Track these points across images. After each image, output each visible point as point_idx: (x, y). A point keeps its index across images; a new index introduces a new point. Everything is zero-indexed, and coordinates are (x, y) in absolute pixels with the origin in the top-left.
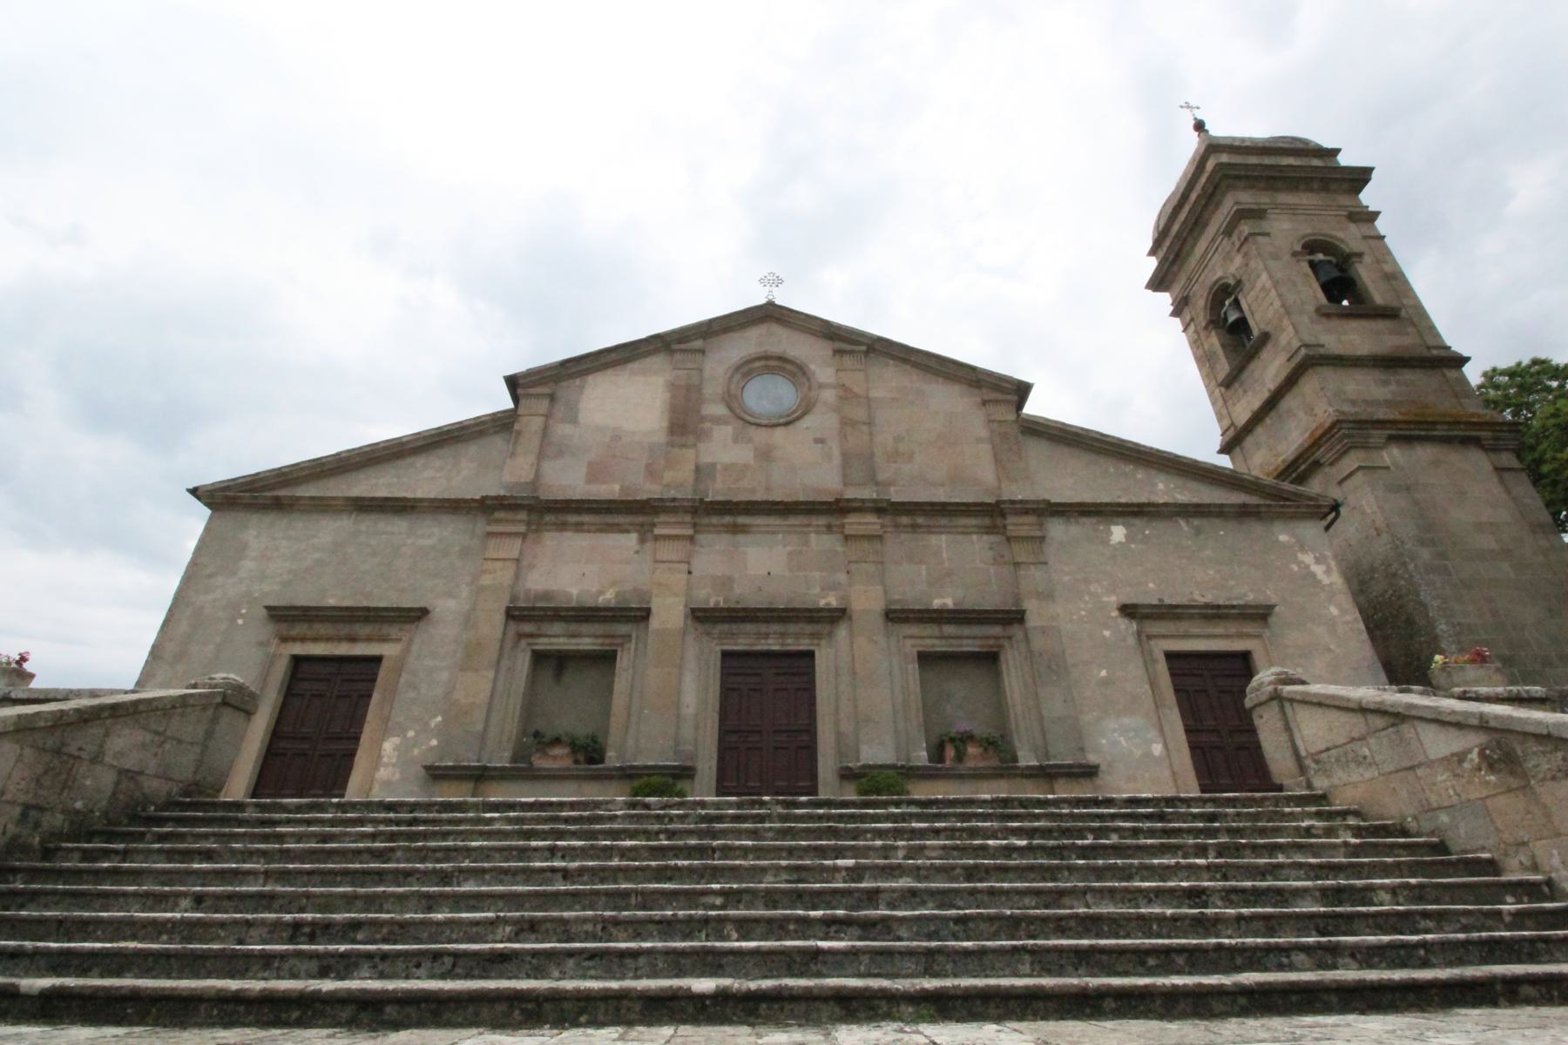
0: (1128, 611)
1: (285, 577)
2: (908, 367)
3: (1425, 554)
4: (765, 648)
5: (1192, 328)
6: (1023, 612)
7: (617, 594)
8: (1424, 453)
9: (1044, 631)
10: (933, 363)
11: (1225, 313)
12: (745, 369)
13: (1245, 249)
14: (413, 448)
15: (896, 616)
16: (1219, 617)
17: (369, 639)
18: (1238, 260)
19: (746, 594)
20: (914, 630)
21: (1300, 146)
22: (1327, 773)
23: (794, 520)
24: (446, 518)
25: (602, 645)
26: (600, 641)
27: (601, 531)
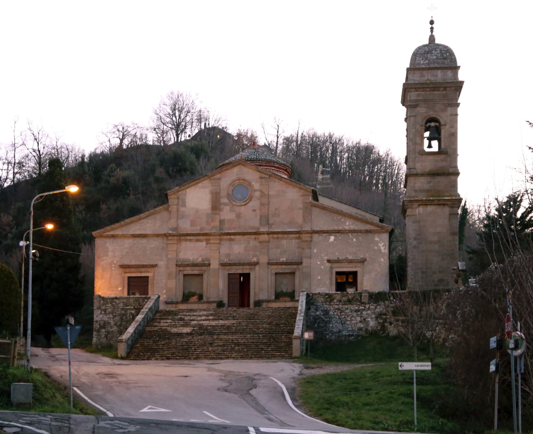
0: (329, 261)
17: (145, 272)
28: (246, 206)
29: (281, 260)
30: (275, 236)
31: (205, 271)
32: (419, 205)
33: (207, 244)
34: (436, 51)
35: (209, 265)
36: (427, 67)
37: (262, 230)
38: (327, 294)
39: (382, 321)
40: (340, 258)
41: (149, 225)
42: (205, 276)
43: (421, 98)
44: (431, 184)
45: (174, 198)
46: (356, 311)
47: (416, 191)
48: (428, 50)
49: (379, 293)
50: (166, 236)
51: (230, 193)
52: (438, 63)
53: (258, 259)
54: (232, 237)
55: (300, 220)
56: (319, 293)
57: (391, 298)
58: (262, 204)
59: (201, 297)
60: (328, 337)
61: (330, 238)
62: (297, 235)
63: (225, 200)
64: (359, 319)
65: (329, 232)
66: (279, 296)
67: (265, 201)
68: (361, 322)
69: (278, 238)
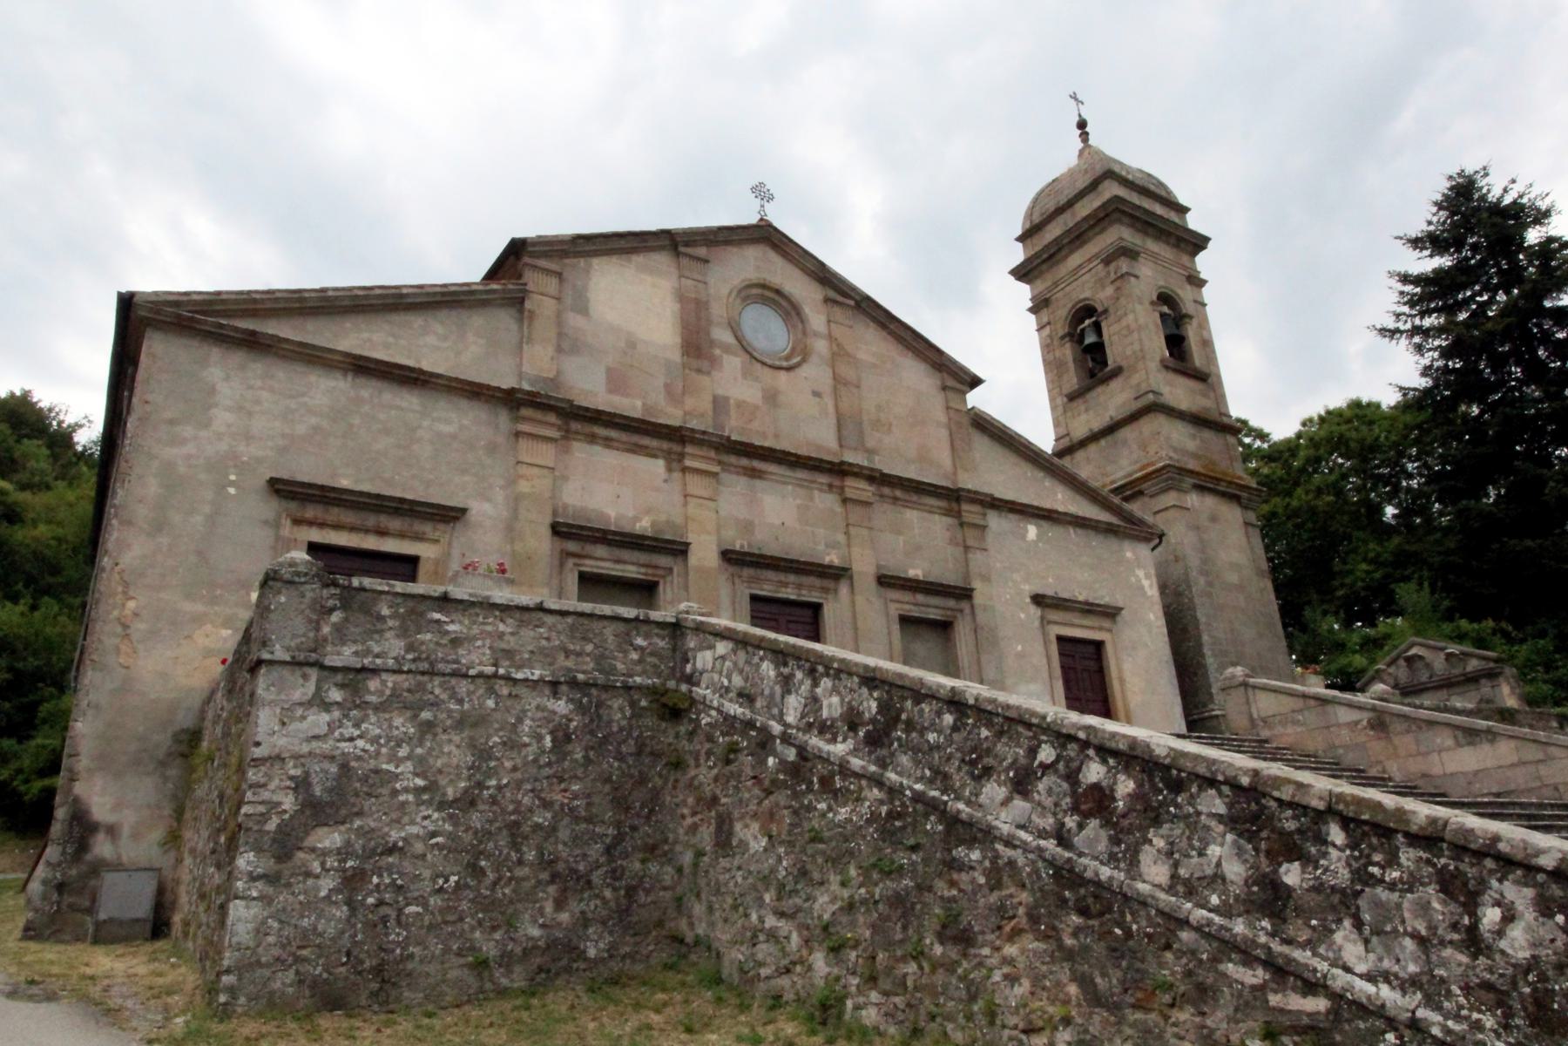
0: (1038, 600)
1: (281, 442)
2: (884, 333)
3: (1202, 581)
4: (785, 596)
5: (1047, 331)
6: (972, 590)
7: (653, 524)
8: (1210, 501)
9: (985, 608)
10: (908, 337)
11: (1083, 330)
12: (743, 294)
13: (1118, 283)
14: (411, 304)
15: (886, 581)
16: (1089, 612)
17: (402, 535)
18: (1110, 290)
19: (766, 541)
20: (907, 596)
21: (1163, 194)
22: (1270, 728)
23: (801, 474)
24: (464, 403)
25: (646, 574)
26: (643, 570)
27: (628, 451)
28: (792, 374)
33: (669, 470)
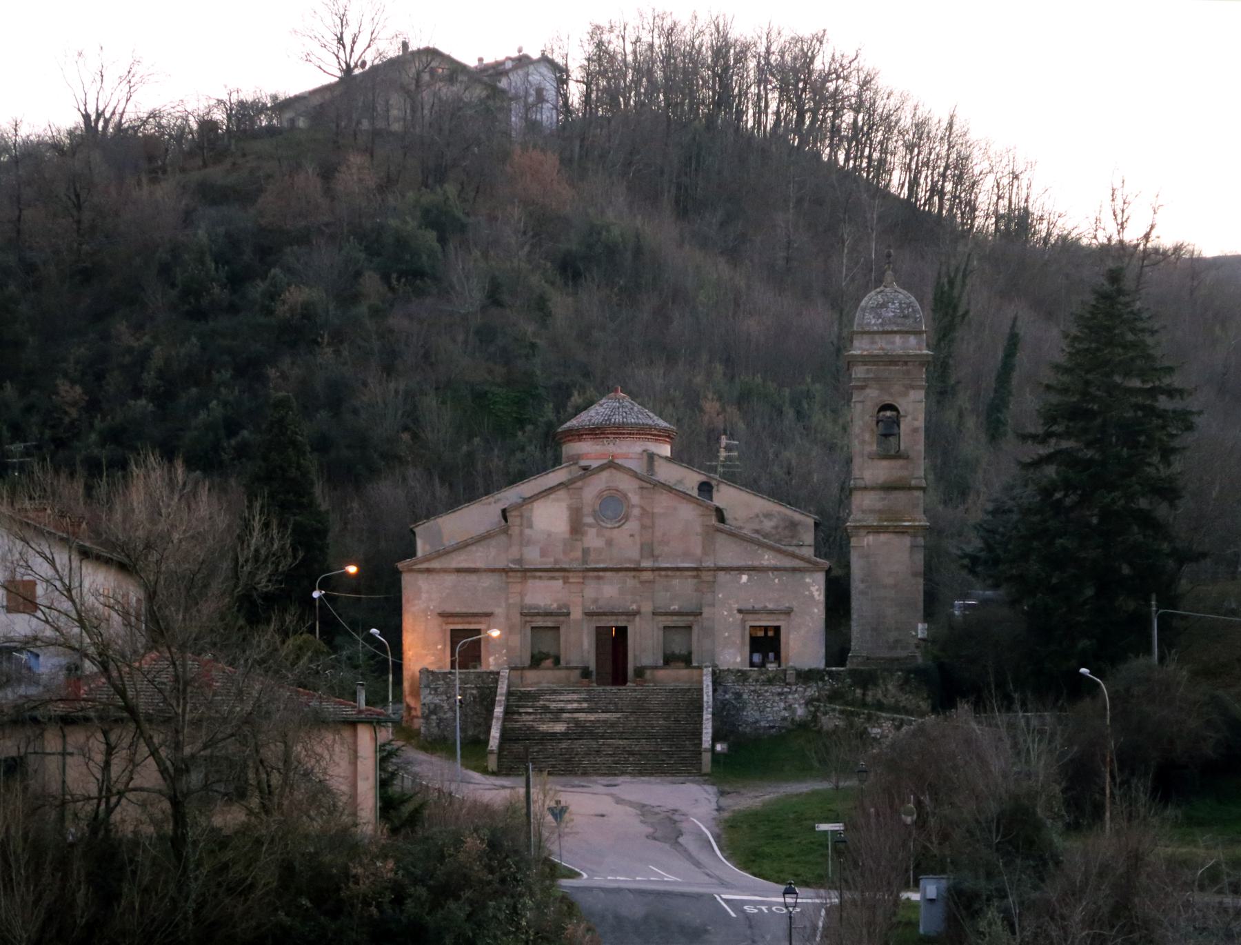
0: (740, 611)
17: (475, 623)
29: (672, 608)
30: (663, 573)
31: (563, 622)
32: (869, 532)
33: (565, 583)
34: (893, 303)
35: (568, 614)
36: (881, 329)
37: (644, 564)
38: (739, 671)
39: (813, 709)
40: (757, 606)
41: (479, 554)
42: (562, 630)
43: (871, 375)
44: (886, 502)
45: (516, 516)
46: (780, 694)
47: (863, 512)
48: (881, 301)
49: (810, 671)
50: (505, 571)
51: (597, 508)
52: (898, 325)
53: (639, 607)
54: (601, 574)
55: (698, 551)
56: (728, 670)
57: (826, 678)
58: (643, 527)
59: (557, 661)
60: (740, 728)
61: (741, 578)
62: (695, 573)
63: (590, 520)
64: (782, 705)
65: (741, 570)
66: (669, 660)
67: (647, 522)
68: (785, 709)
69: (667, 576)
